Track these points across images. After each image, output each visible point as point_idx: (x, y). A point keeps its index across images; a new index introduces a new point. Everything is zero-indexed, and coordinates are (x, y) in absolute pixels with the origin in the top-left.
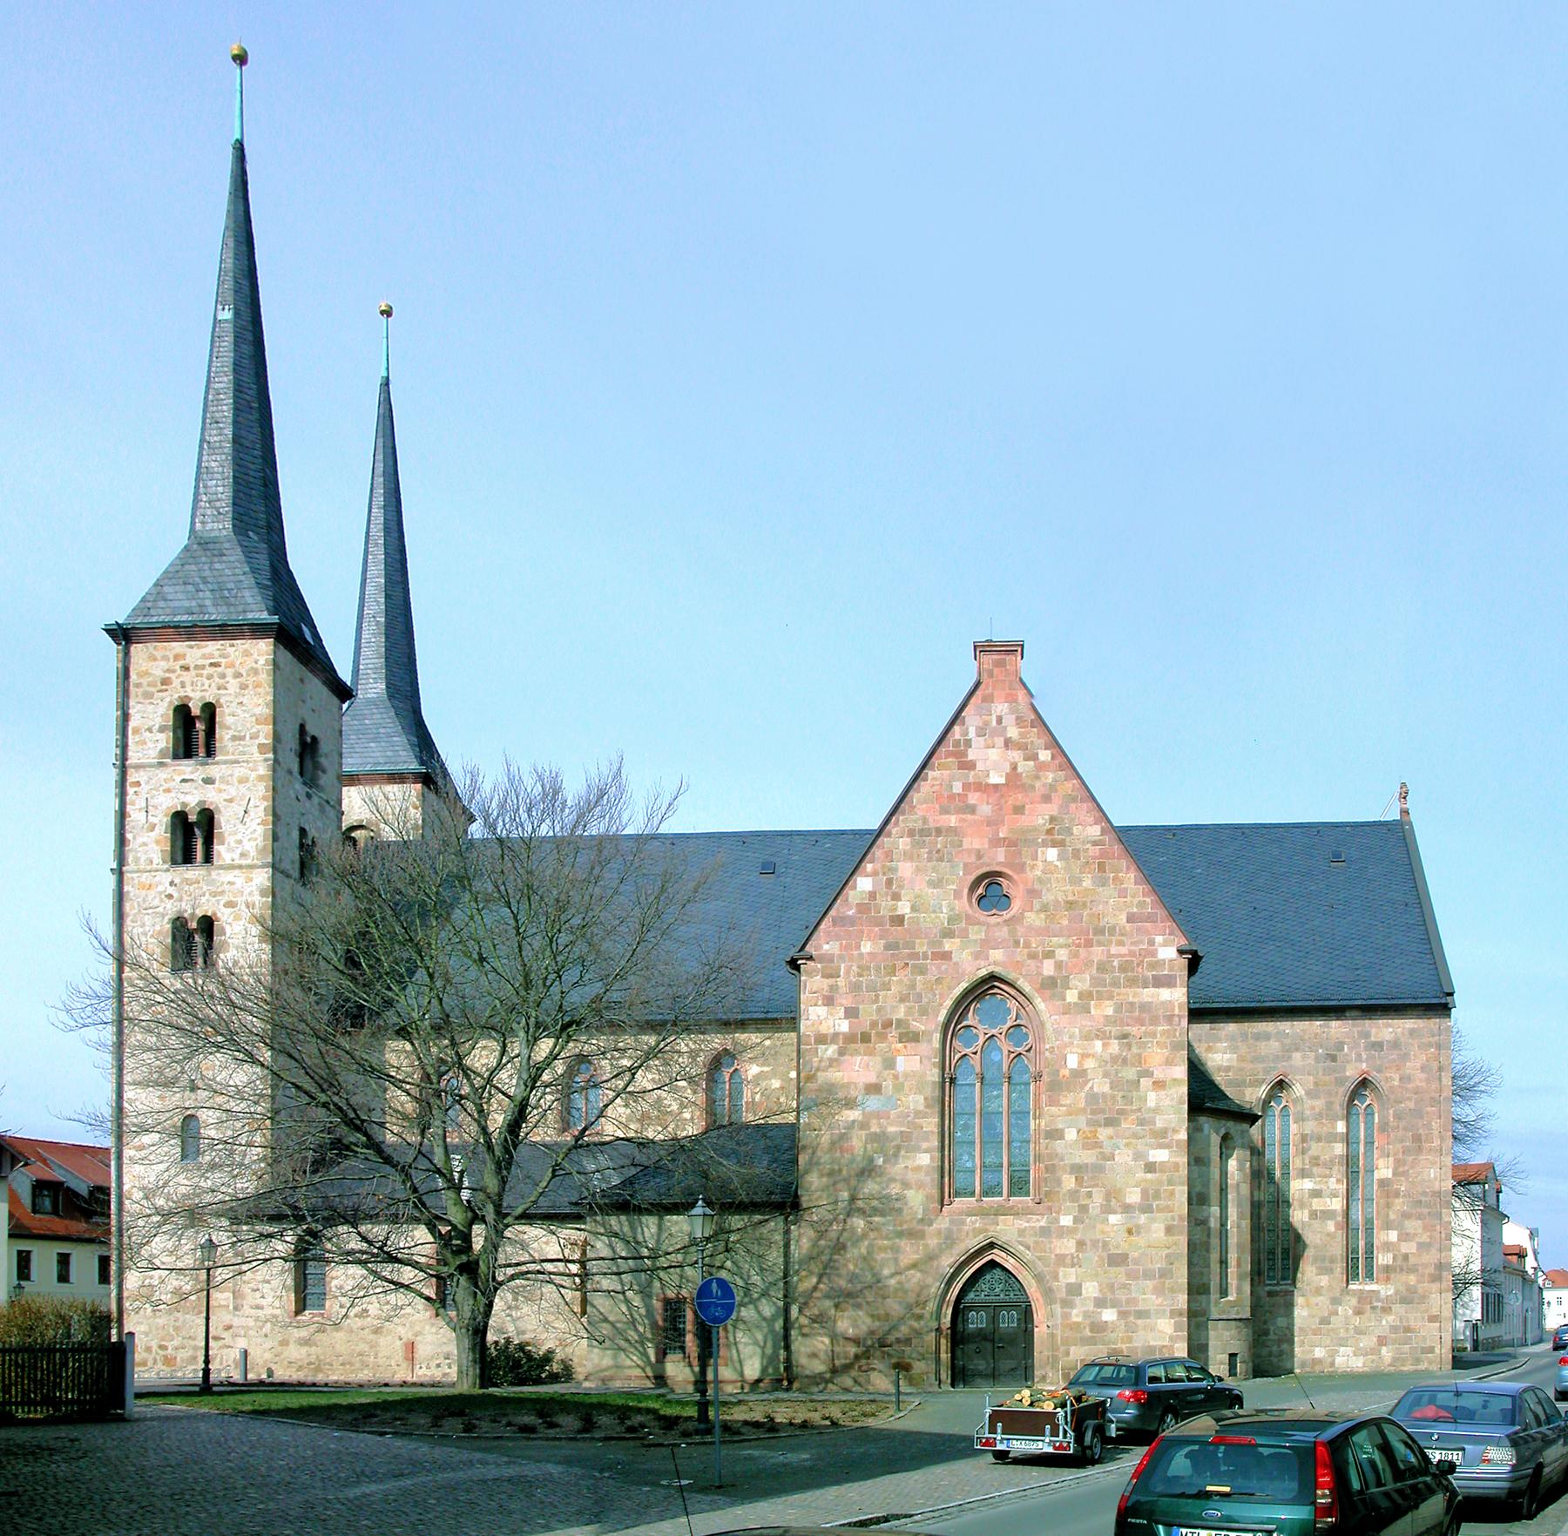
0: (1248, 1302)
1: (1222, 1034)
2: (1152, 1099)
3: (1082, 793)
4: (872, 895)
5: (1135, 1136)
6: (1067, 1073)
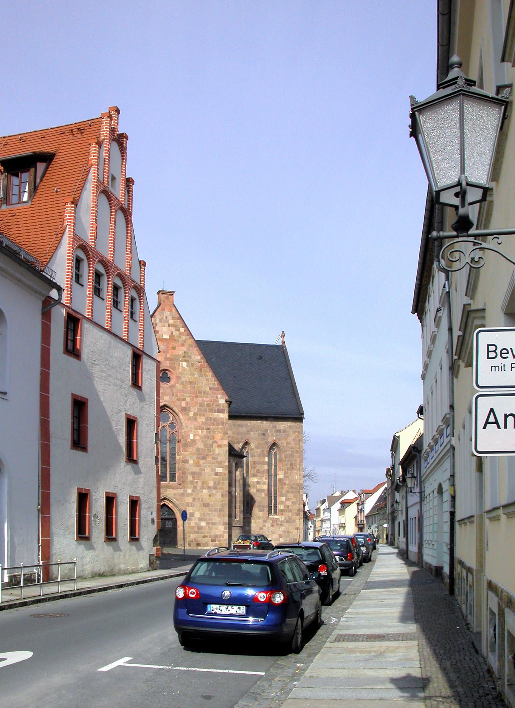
0: (242, 521)
2: (217, 451)
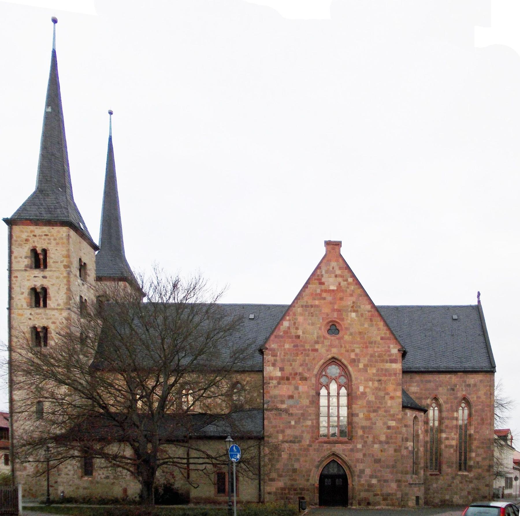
1: (414, 380)
2: (389, 403)
4: (289, 328)
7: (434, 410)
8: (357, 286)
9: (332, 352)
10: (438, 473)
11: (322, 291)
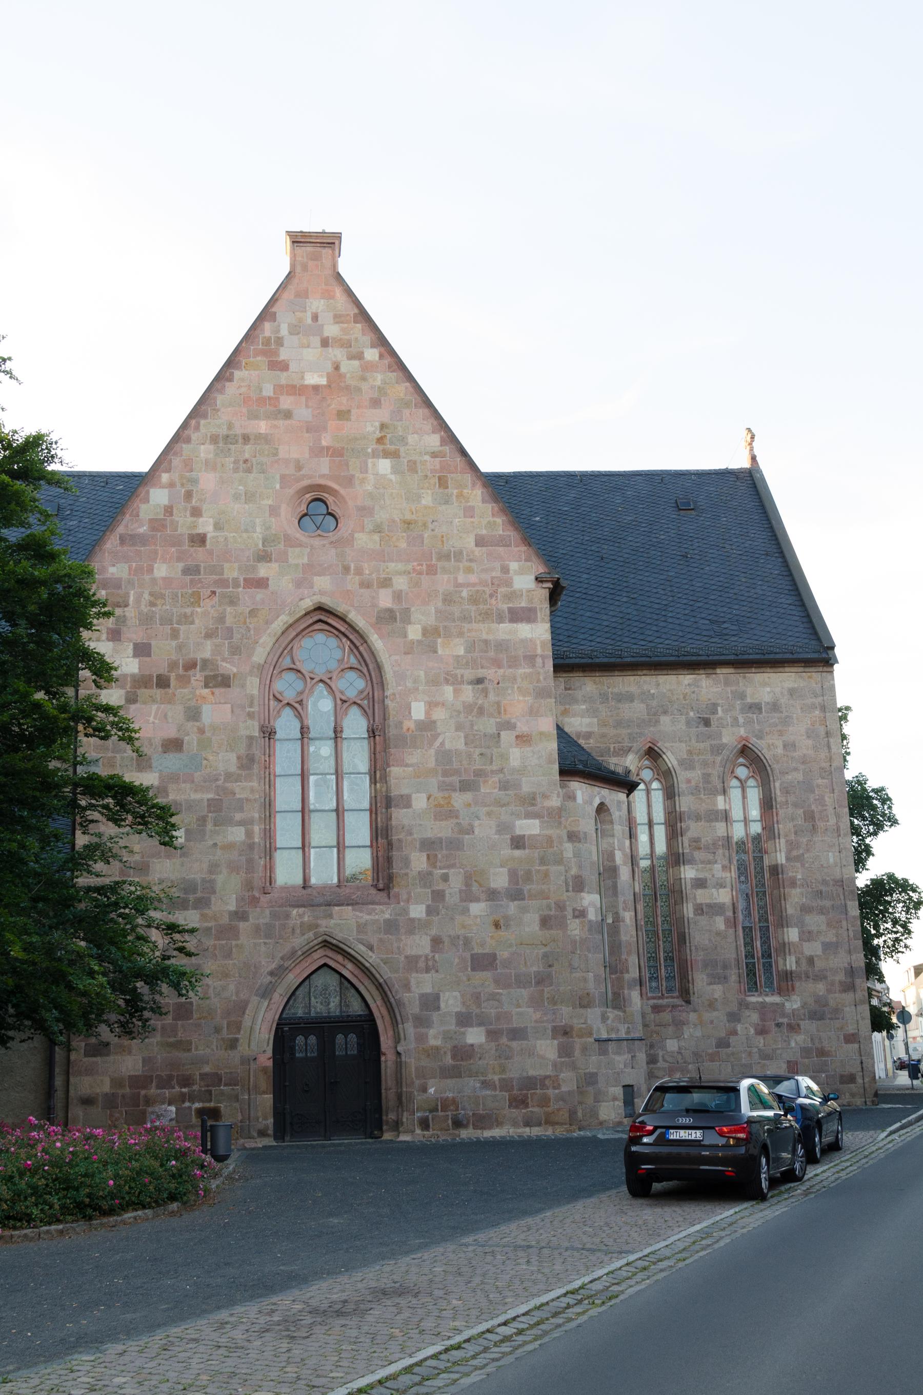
1: (579, 694)
2: (516, 756)
3: (414, 398)
4: (169, 510)
5: (500, 804)
6: (412, 725)
7: (648, 791)
8: (393, 375)
9: (316, 589)
10: (679, 1002)
11: (280, 389)
